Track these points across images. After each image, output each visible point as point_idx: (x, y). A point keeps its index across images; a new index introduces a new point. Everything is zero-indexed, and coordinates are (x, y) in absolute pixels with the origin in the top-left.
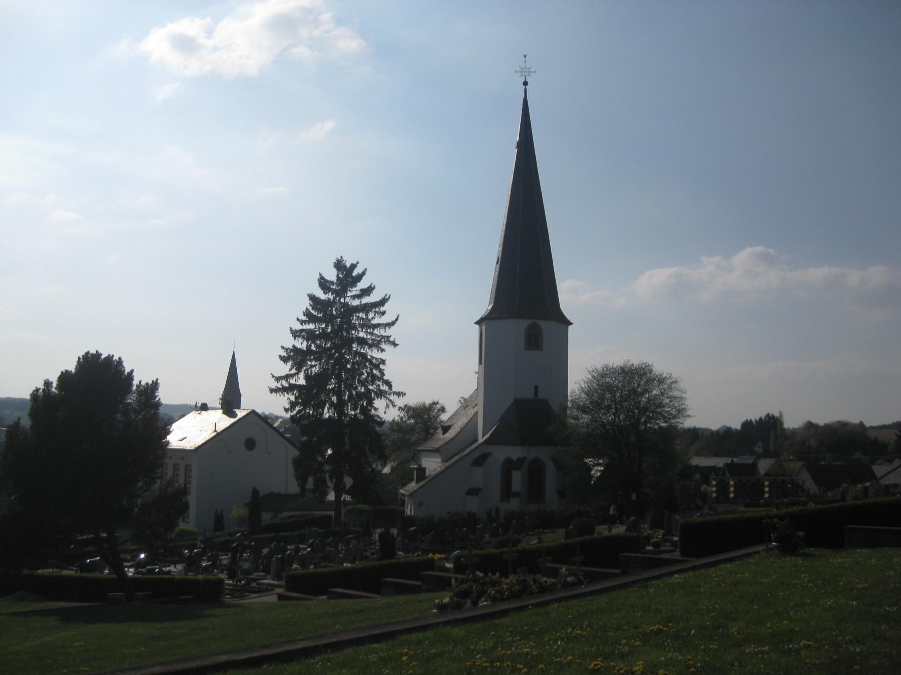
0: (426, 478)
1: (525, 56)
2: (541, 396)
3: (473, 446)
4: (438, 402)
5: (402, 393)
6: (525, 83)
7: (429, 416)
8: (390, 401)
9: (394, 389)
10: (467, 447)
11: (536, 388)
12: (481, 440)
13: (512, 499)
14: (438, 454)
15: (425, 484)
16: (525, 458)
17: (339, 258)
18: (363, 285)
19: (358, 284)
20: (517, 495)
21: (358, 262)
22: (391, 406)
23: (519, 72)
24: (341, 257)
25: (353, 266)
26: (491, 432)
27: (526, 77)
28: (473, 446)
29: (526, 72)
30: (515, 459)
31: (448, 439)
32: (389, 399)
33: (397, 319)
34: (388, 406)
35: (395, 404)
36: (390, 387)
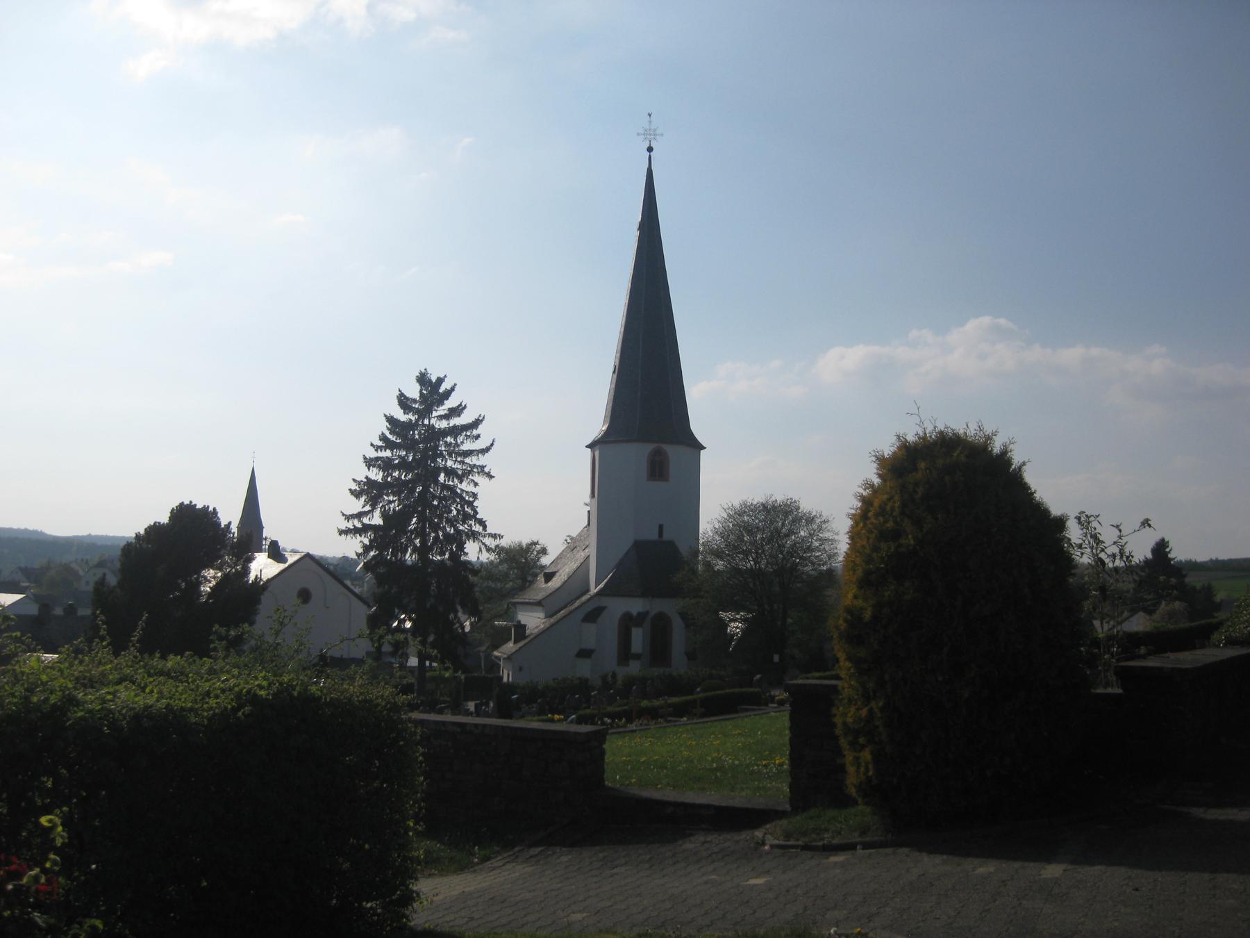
1: (650, 115)
2: (666, 537)
3: (584, 598)
5: (499, 535)
6: (650, 149)
8: (484, 544)
9: (489, 530)
11: (661, 527)
14: (540, 608)
15: (525, 645)
16: (647, 613)
20: (637, 657)
25: (440, 381)
28: (584, 598)
29: (651, 134)
33: (492, 445)
34: (481, 550)
36: (485, 527)
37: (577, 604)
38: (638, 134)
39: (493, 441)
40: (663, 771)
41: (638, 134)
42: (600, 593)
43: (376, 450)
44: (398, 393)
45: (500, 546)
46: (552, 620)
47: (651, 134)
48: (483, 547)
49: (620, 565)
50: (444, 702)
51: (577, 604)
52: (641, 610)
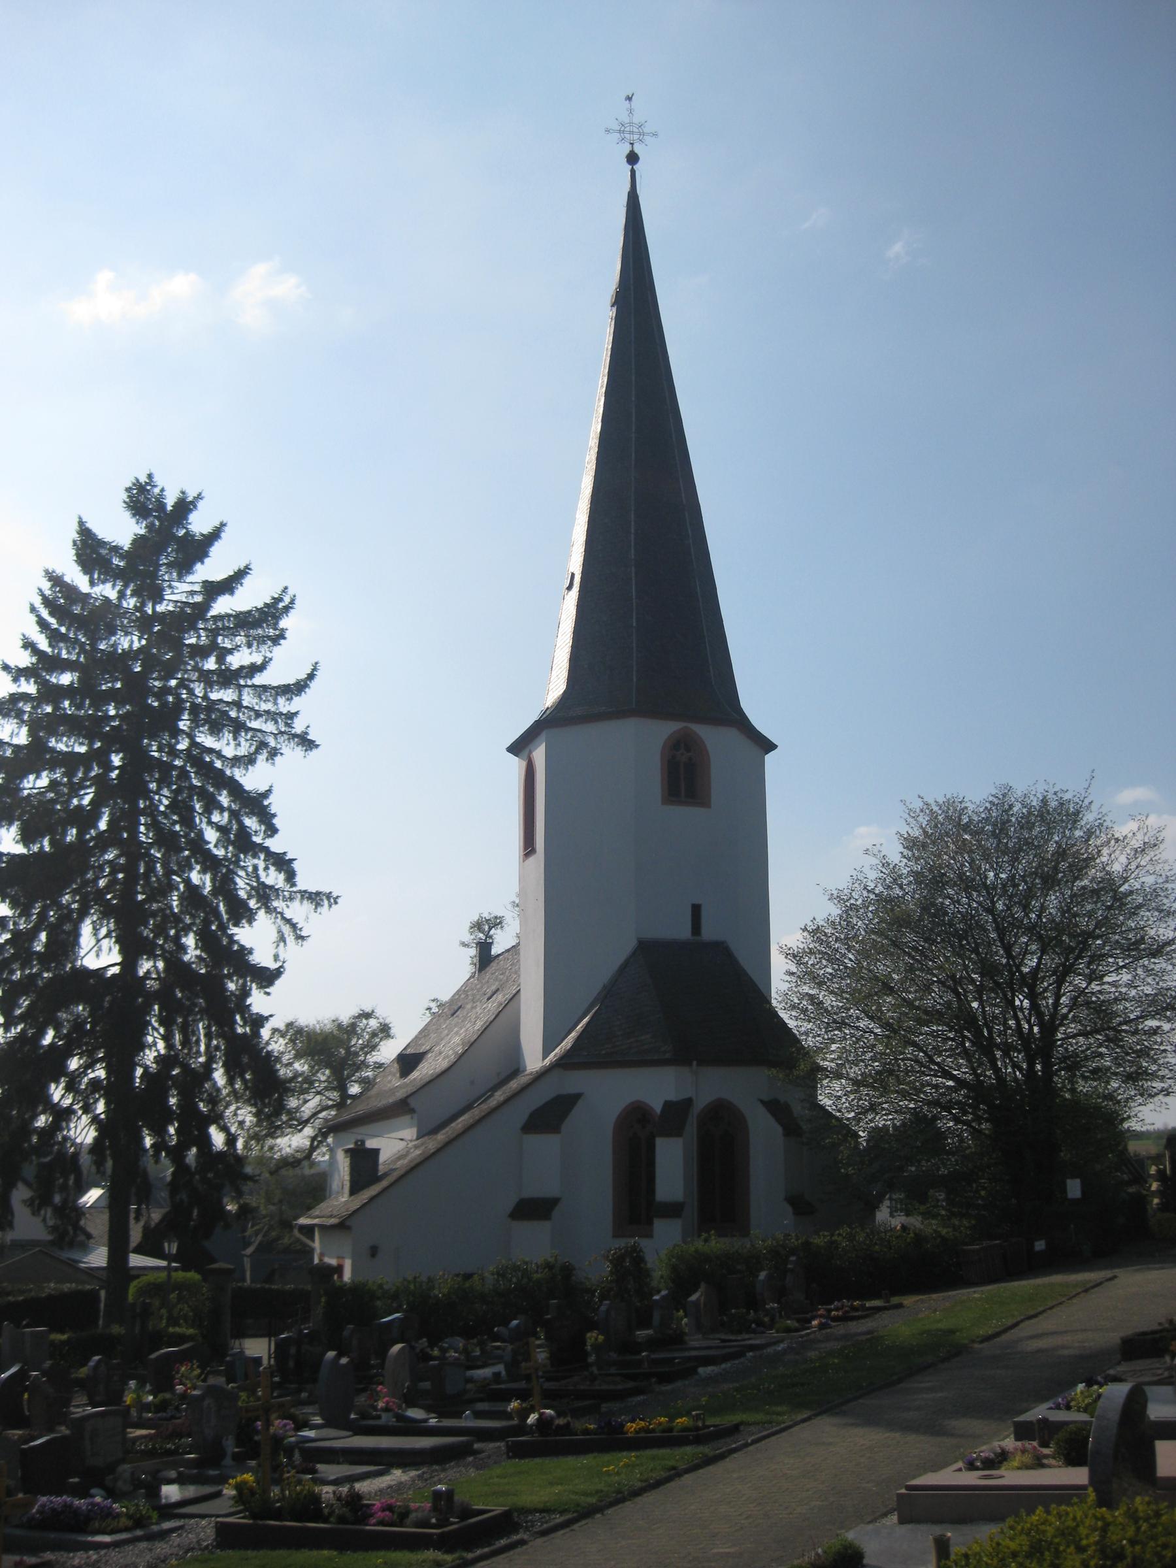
0: (378, 1179)
1: (629, 99)
2: (709, 932)
3: (514, 1085)
4: (373, 1011)
5: (329, 896)
6: (633, 158)
7: (348, 1049)
8: (288, 921)
9: (304, 882)
10: (495, 1089)
11: (696, 910)
12: (534, 1059)
13: (659, 1225)
14: (406, 1119)
15: (372, 1199)
16: (689, 1102)
17: (143, 479)
18: (212, 569)
19: (198, 566)
20: (673, 1210)
21: (200, 494)
22: (290, 939)
23: (615, 131)
24: (150, 476)
25: (185, 507)
26: (573, 1035)
27: (632, 144)
28: (514, 1085)
29: (631, 133)
30: (657, 1107)
31: (419, 1084)
32: (284, 918)
33: (311, 676)
34: (282, 939)
35: (303, 934)
36: (291, 876)
37: (499, 1096)
38: (608, 131)
39: (315, 668)
40: (381, 1391)
41: (608, 131)
42: (564, 1063)
43: (16, 680)
44: (72, 533)
45: (297, 1024)
46: (432, 1144)
47: (631, 133)
48: (286, 929)
49: (609, 996)
50: (179, 1339)
51: (499, 1096)
52: (672, 1096)
